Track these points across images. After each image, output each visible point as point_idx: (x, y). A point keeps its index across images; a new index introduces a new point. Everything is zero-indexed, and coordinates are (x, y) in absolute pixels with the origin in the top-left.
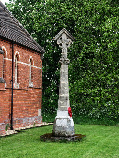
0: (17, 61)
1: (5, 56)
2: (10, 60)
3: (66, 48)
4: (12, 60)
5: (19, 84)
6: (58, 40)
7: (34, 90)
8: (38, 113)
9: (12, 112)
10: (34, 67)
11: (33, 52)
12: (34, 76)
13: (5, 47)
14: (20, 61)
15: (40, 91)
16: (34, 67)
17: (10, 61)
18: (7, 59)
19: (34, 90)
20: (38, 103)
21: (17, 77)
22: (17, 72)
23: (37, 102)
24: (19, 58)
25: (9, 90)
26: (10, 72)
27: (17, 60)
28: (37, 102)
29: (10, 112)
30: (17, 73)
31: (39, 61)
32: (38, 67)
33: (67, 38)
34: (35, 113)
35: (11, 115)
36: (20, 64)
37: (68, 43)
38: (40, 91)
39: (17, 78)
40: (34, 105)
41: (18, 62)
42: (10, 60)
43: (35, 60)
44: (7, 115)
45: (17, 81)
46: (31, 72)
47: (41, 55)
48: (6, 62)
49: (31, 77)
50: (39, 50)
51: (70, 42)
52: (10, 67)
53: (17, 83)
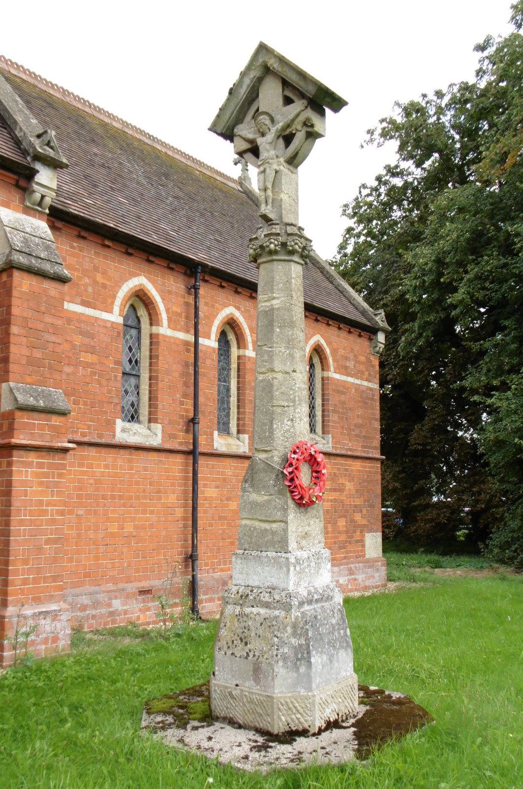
0: (239, 348)
1: (153, 317)
2: (181, 335)
3: (282, 160)
4: (191, 338)
5: (245, 437)
6: (240, 127)
7: (336, 464)
8: (363, 546)
9: (194, 547)
10: (337, 376)
11: (328, 321)
12: (334, 411)
13: (322, 336)
14: (165, 322)
15: (373, 467)
16: (337, 376)
17: (187, 343)
18: (164, 330)
19: (336, 464)
20: (361, 511)
21: (238, 407)
22: (238, 389)
23: (357, 509)
24: (326, 358)
25: (179, 459)
26: (186, 384)
27: (238, 343)
28: (357, 509)
29: (184, 546)
30: (238, 395)
31: (362, 359)
32: (365, 383)
33: (288, 101)
34: (344, 547)
35: (191, 559)
36: (333, 379)
37: (287, 132)
38: (373, 467)
39: (238, 413)
40: (341, 517)
41: (241, 352)
42: (181, 335)
43: (342, 352)
44: (175, 554)
45: (238, 425)
46: (323, 395)
47: (370, 339)
48: (158, 343)
49: (323, 416)
50: (364, 321)
51: (302, 118)
52: (187, 365)
53: (239, 432)
